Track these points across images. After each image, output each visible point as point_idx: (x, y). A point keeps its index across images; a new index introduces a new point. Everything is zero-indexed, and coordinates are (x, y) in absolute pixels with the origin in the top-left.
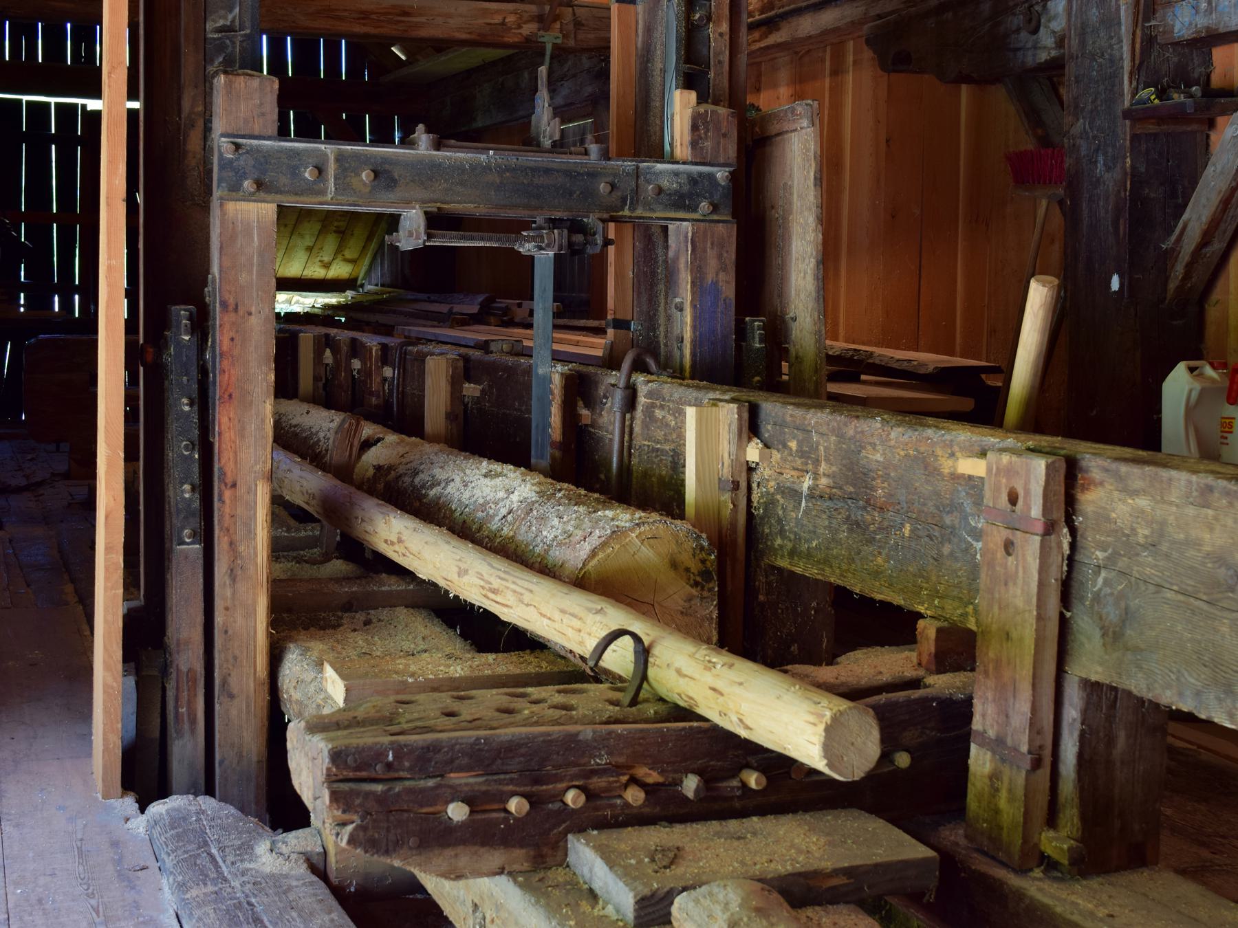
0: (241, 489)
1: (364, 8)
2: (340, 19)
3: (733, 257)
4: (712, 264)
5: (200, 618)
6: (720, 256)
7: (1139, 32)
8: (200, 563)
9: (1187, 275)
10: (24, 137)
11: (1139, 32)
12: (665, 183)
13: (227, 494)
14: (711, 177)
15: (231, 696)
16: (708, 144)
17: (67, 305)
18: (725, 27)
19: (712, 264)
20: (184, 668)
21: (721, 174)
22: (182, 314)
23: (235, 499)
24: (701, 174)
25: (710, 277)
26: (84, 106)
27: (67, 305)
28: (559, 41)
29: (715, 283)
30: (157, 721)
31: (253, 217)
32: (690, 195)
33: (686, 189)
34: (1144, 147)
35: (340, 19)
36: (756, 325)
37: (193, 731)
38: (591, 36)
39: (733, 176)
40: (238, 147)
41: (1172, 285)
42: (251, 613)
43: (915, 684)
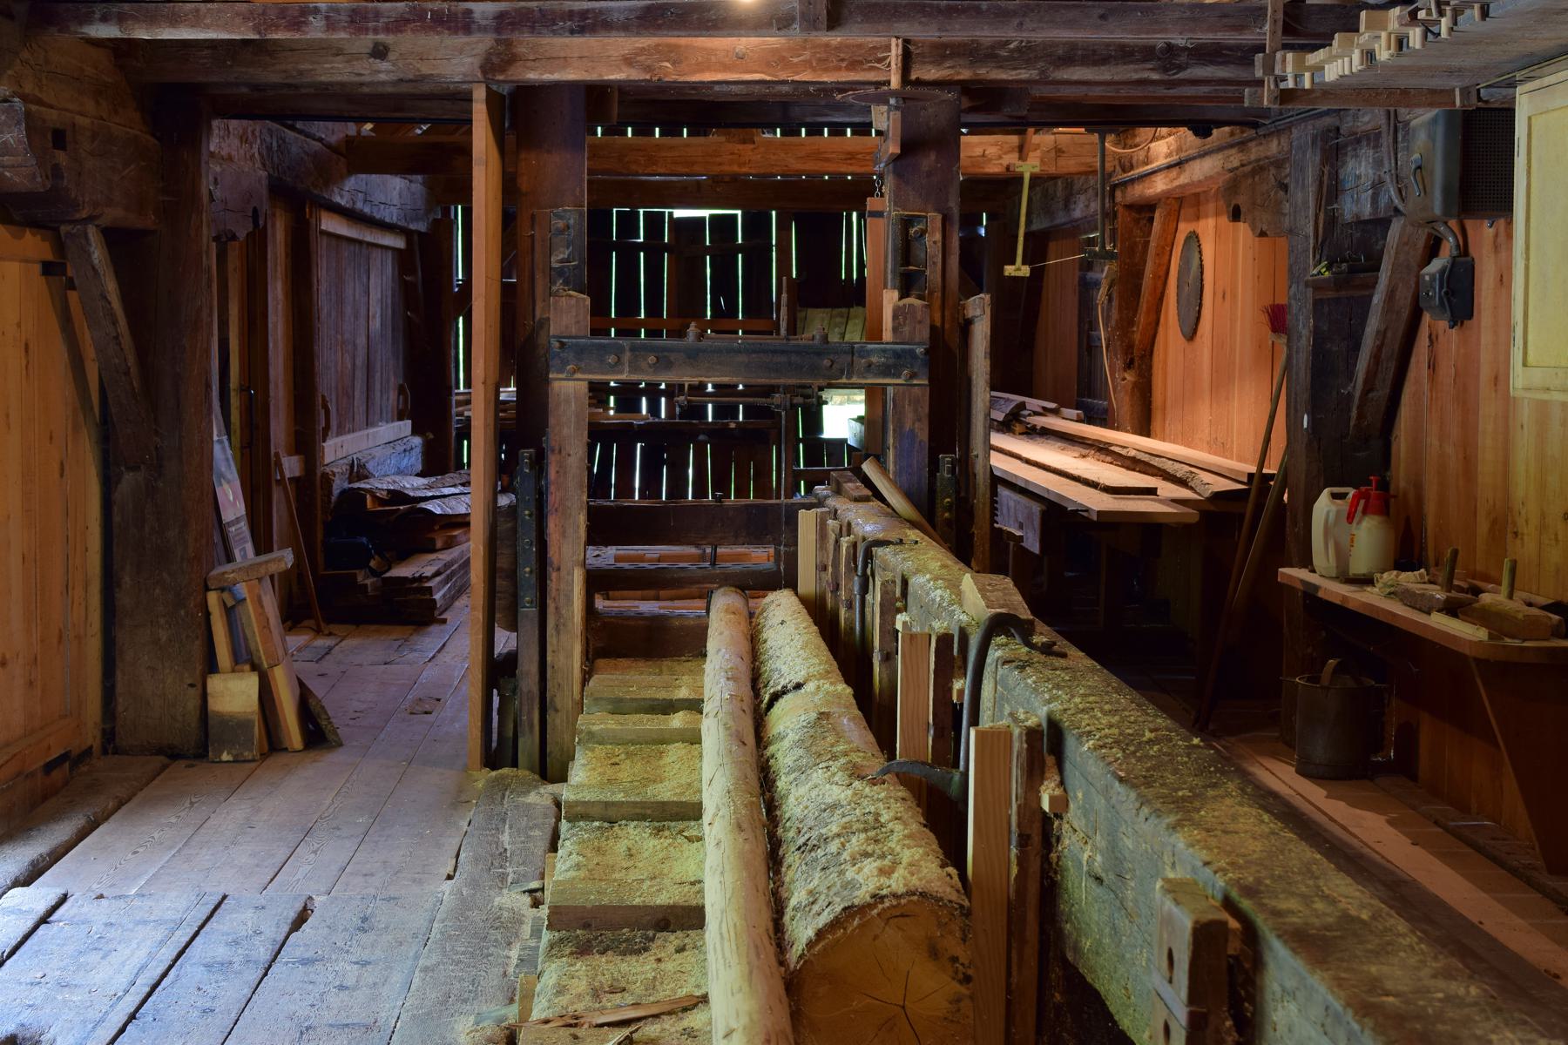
0: (563, 572)
1: (850, 149)
2: (827, 160)
3: (927, 410)
4: (909, 416)
5: (536, 658)
6: (915, 411)
7: (1322, 216)
8: (536, 620)
9: (1360, 416)
10: (615, 246)
11: (1322, 216)
12: (874, 359)
13: (554, 575)
14: (912, 352)
15: (557, 711)
16: (906, 329)
17: (654, 409)
18: (938, 236)
19: (909, 416)
20: (525, 690)
21: (920, 350)
22: (526, 454)
23: (559, 579)
24: (903, 351)
25: (907, 427)
26: (671, 214)
27: (654, 409)
28: (1037, 170)
29: (912, 431)
30: (511, 726)
31: (571, 390)
32: (895, 366)
33: (891, 361)
34: (1326, 309)
35: (827, 160)
36: (946, 459)
37: (531, 731)
38: (1072, 162)
39: (927, 352)
40: (562, 345)
41: (1352, 423)
42: (570, 656)
43: (974, 721)
